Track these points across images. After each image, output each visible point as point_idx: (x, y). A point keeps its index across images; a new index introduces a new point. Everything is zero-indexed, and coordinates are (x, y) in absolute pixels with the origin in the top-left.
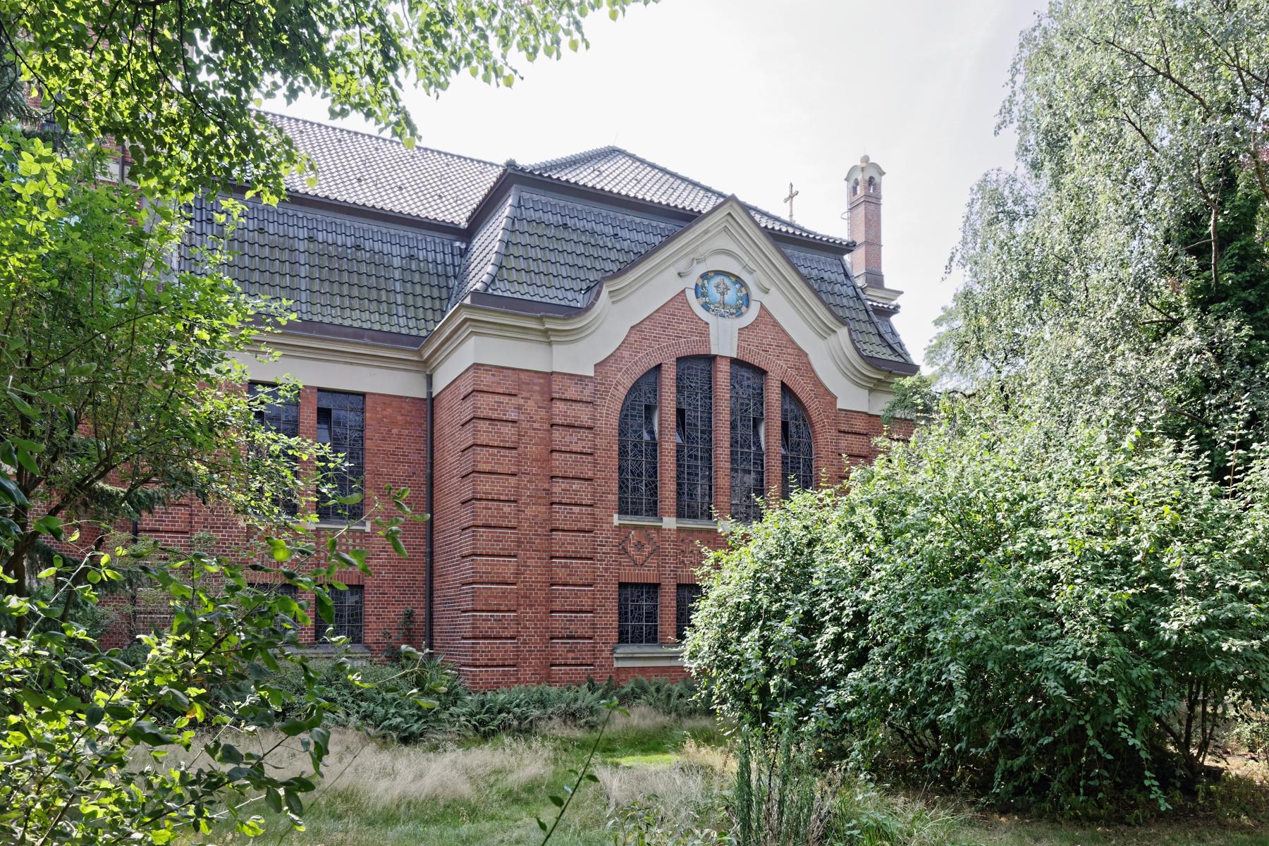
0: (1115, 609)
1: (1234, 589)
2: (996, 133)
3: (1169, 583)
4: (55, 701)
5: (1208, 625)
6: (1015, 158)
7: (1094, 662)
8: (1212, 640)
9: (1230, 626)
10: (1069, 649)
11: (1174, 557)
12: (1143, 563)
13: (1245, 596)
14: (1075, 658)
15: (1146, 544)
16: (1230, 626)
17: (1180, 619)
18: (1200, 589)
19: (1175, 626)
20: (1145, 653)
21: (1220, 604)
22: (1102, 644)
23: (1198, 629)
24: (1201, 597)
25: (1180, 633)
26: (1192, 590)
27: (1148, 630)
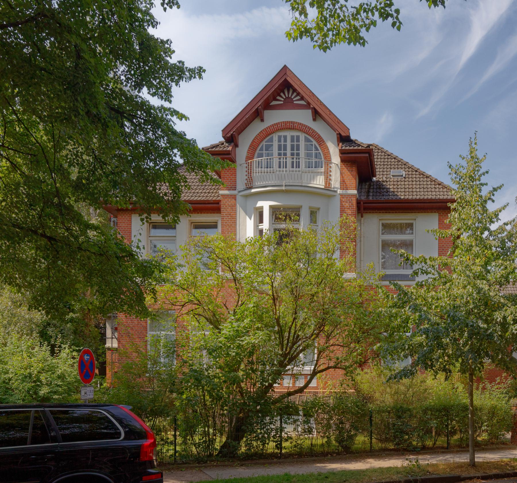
0: (28, 388)
1: (56, 384)
2: (187, 118)
3: (41, 382)
4: (132, 140)
5: (50, 392)
6: (291, 12)
7: (23, 400)
8: (51, 396)
9: (55, 393)
10: (17, 397)
11: (43, 377)
12: (35, 377)
13: (58, 386)
14: (19, 399)
15: (36, 372)
16: (55, 393)
17: (44, 391)
18: (49, 384)
19: (43, 392)
20: (35, 399)
21: (53, 387)
22: (25, 396)
23: (48, 393)
24: (49, 386)
25: (44, 394)
26: (47, 384)
27: (36, 393)
